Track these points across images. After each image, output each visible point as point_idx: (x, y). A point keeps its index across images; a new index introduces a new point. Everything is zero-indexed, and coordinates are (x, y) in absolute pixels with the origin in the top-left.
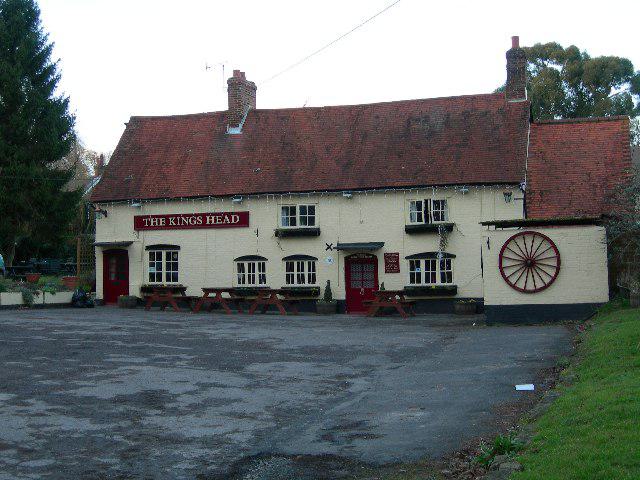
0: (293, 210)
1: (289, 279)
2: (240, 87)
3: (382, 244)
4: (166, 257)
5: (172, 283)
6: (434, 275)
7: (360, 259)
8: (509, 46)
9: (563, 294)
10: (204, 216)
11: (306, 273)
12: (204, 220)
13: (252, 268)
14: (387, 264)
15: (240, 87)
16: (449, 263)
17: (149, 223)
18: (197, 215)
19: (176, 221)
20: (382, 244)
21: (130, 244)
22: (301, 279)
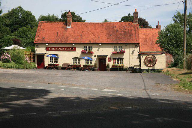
0: (86, 47)
1: (74, 63)
2: (136, 13)
3: (108, 56)
4: (54, 58)
5: (56, 63)
6: (86, 62)
7: (102, 60)
8: (134, 11)
9: (157, 67)
10: (65, 48)
11: (78, 61)
12: (65, 49)
13: (76, 60)
14: (108, 60)
15: (136, 13)
16: (57, 60)
17: (50, 49)
18: (63, 47)
19: (57, 49)
20: (108, 56)
21: (45, 54)
22: (76, 63)
